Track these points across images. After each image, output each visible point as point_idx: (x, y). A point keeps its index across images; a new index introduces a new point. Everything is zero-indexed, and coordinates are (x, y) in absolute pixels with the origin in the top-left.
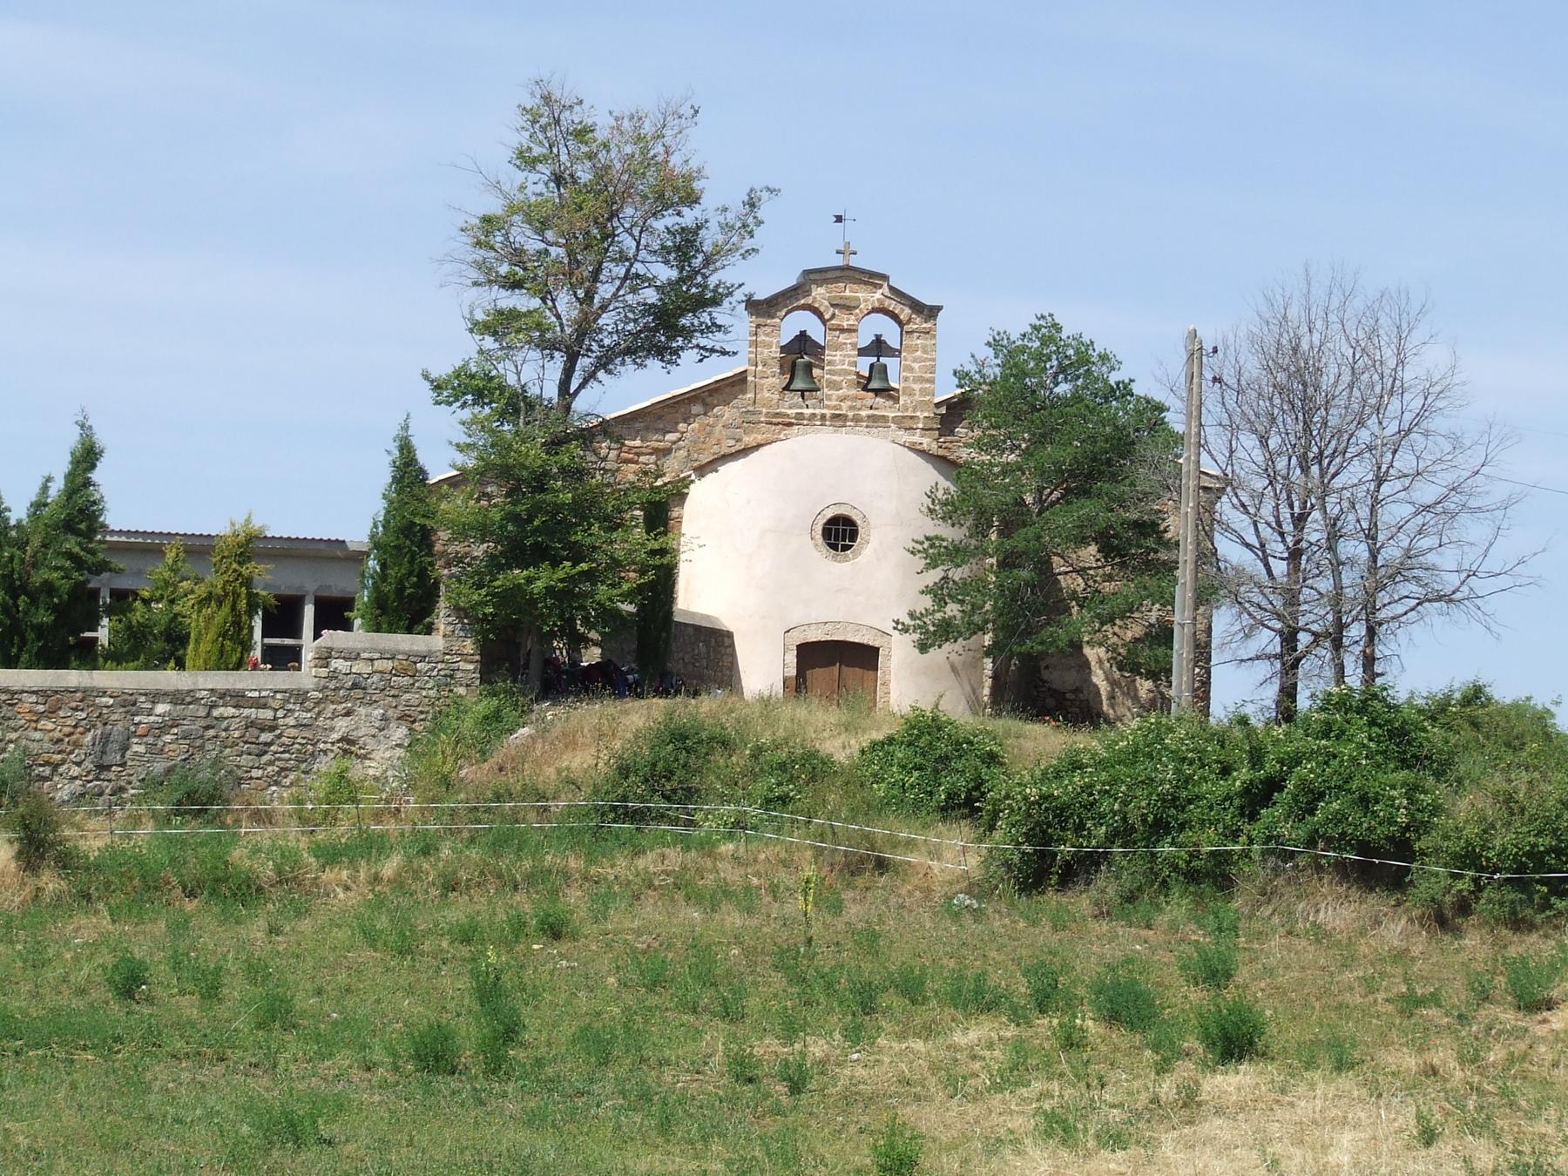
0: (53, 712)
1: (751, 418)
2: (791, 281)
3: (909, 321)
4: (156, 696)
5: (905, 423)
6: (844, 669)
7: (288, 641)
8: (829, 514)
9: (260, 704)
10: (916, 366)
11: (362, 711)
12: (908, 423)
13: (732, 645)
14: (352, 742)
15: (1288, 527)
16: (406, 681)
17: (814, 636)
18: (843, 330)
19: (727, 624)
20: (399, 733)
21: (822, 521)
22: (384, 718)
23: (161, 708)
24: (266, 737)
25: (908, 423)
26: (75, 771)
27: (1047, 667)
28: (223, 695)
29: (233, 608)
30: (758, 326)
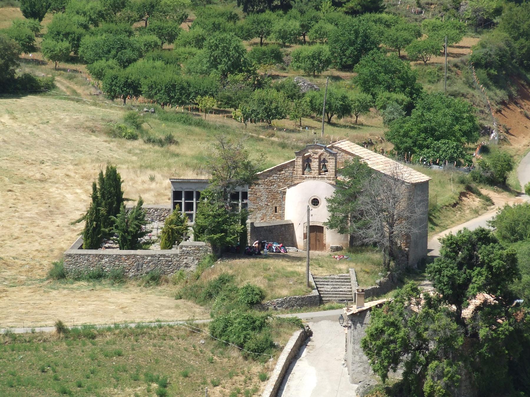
0: (128, 259)
4: (148, 256)
8: (313, 198)
9: (169, 257)
11: (189, 258)
14: (187, 264)
16: (198, 251)
20: (196, 262)
22: (193, 259)
23: (149, 258)
24: (170, 263)
26: (133, 271)
28: (161, 255)
29: (168, 234)
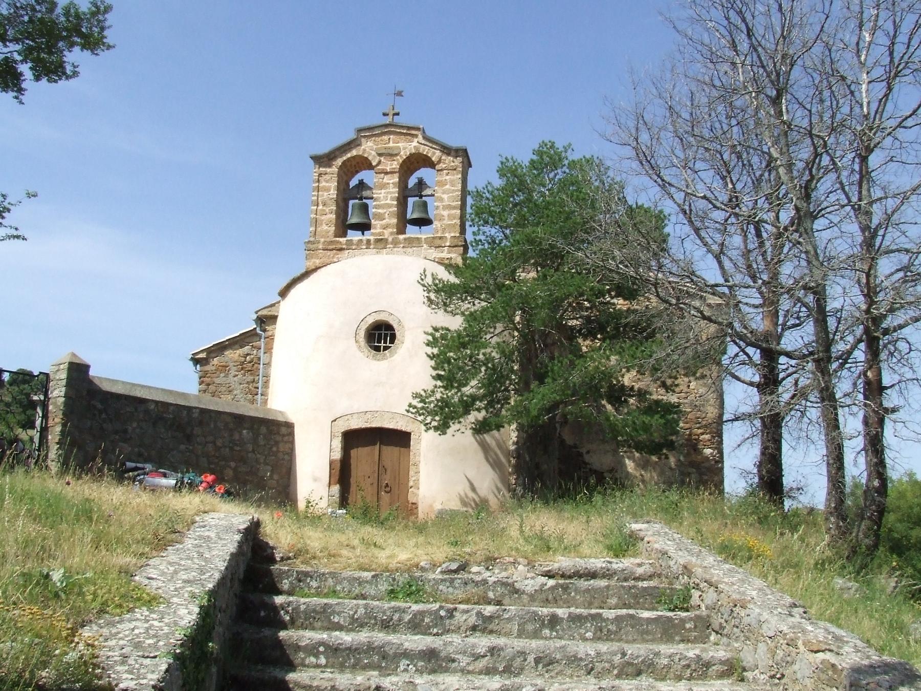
1: (311, 246)
2: (352, 135)
3: (439, 162)
5: (436, 243)
6: (384, 448)
7: (54, 452)
8: (370, 320)
10: (445, 196)
12: (438, 242)
13: (292, 434)
15: (759, 263)
17: (356, 424)
18: (386, 173)
19: (292, 418)
21: (364, 326)
25: (438, 242)
27: (588, 452)
30: (320, 175)
